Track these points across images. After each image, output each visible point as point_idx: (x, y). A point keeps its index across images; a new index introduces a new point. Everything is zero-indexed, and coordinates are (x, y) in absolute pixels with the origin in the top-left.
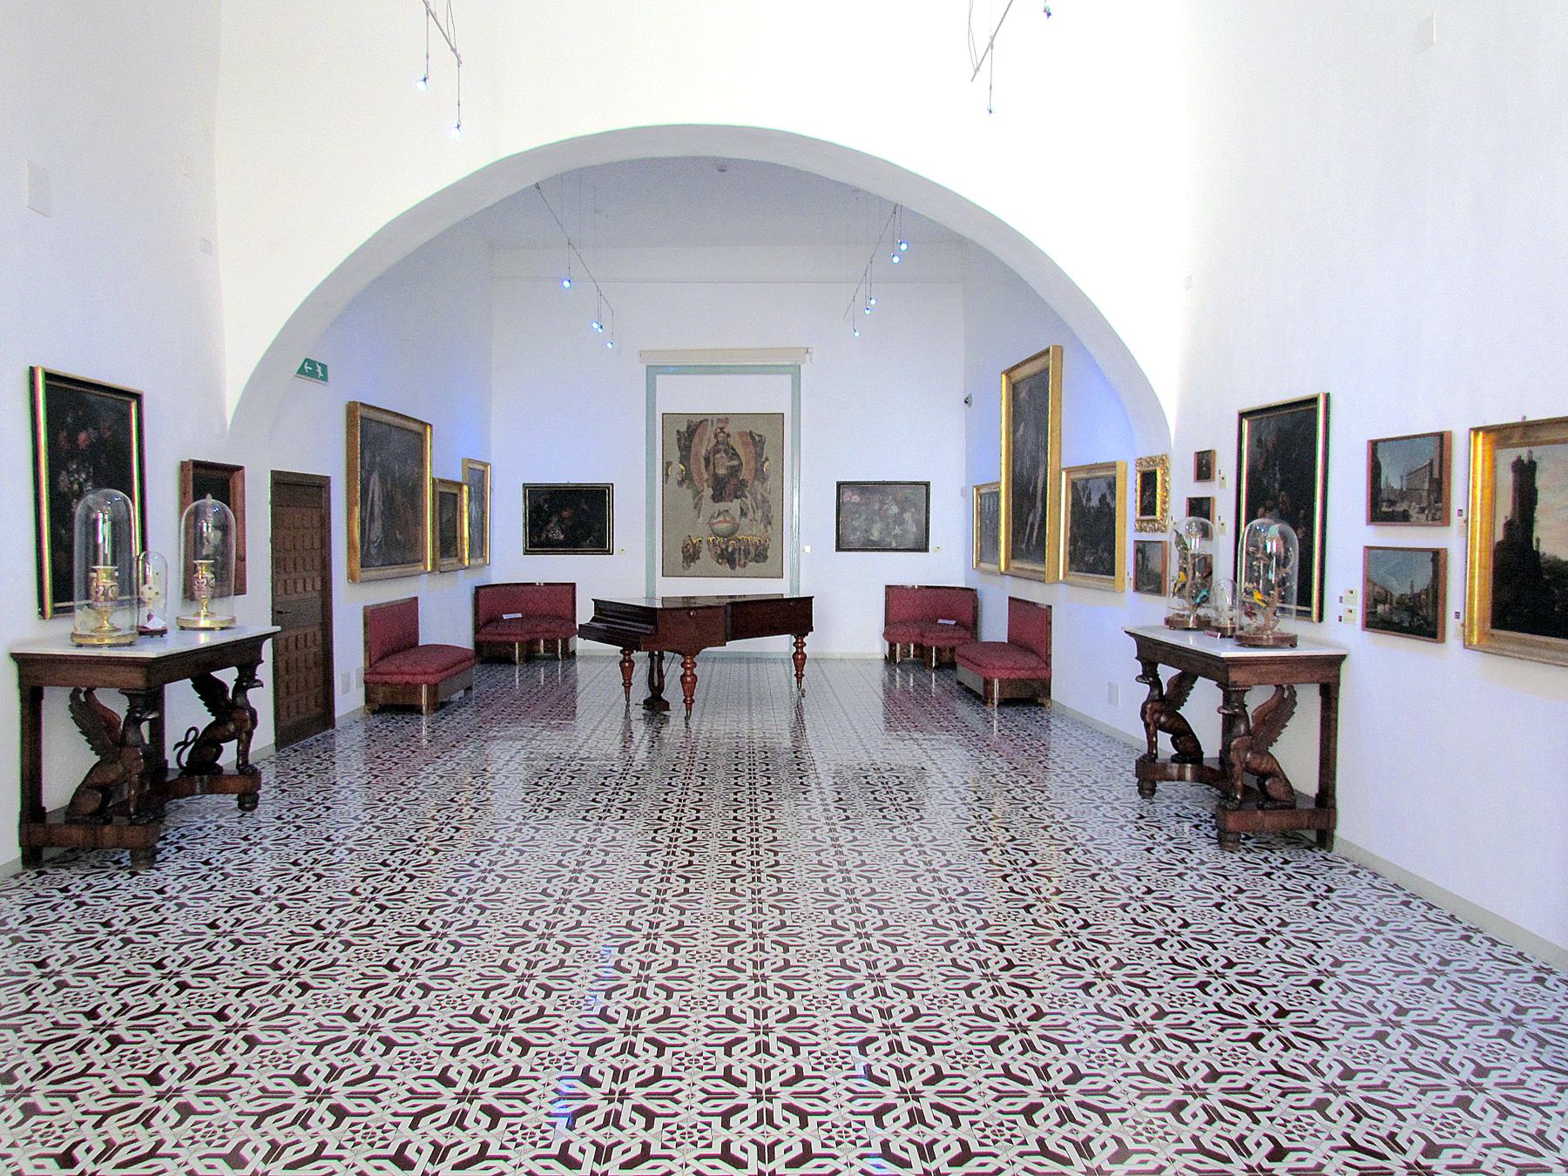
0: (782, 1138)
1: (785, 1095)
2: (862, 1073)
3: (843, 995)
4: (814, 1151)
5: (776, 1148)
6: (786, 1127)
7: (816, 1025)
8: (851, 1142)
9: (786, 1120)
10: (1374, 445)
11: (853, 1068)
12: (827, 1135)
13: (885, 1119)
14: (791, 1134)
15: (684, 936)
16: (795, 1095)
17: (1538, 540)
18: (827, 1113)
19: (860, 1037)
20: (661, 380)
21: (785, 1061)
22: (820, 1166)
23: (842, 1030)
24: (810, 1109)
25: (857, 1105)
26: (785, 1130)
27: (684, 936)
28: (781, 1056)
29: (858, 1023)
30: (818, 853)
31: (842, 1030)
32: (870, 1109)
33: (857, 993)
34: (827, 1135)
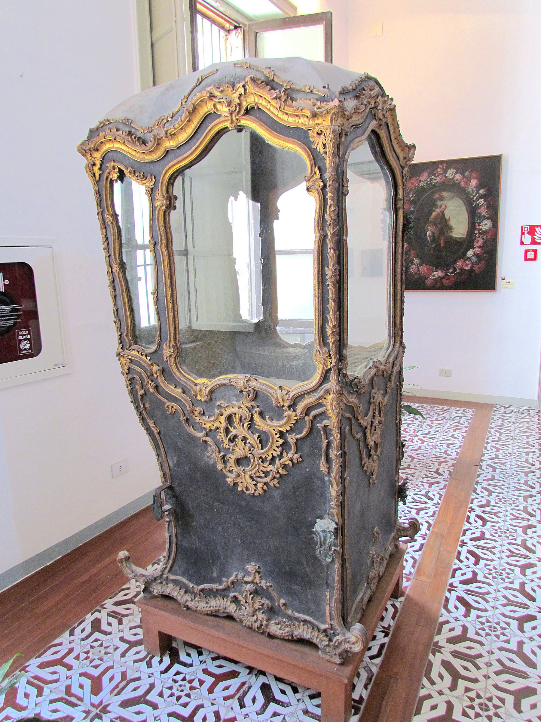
0: (462, 567)
1: (461, 589)
2: (518, 587)
3: (519, 530)
4: (469, 635)
5: (425, 702)
6: (455, 613)
7: (495, 547)
8: (506, 537)
9: (468, 558)
10: (522, 227)
11: (512, 583)
12: (488, 572)
13: (526, 625)
14: (467, 566)
15: (441, 457)
16: (476, 546)
17: (384, 239)
18: (485, 610)
19: (523, 561)
20: (319, 30)
21: (467, 566)
22: (470, 648)
23: (512, 554)
24: (475, 605)
25: (507, 610)
26: (437, 687)
27: (441, 457)
28: (466, 562)
29: (524, 552)
30: (527, 437)
31: (512, 554)
32: (516, 615)
33: (529, 531)
34: (488, 572)
